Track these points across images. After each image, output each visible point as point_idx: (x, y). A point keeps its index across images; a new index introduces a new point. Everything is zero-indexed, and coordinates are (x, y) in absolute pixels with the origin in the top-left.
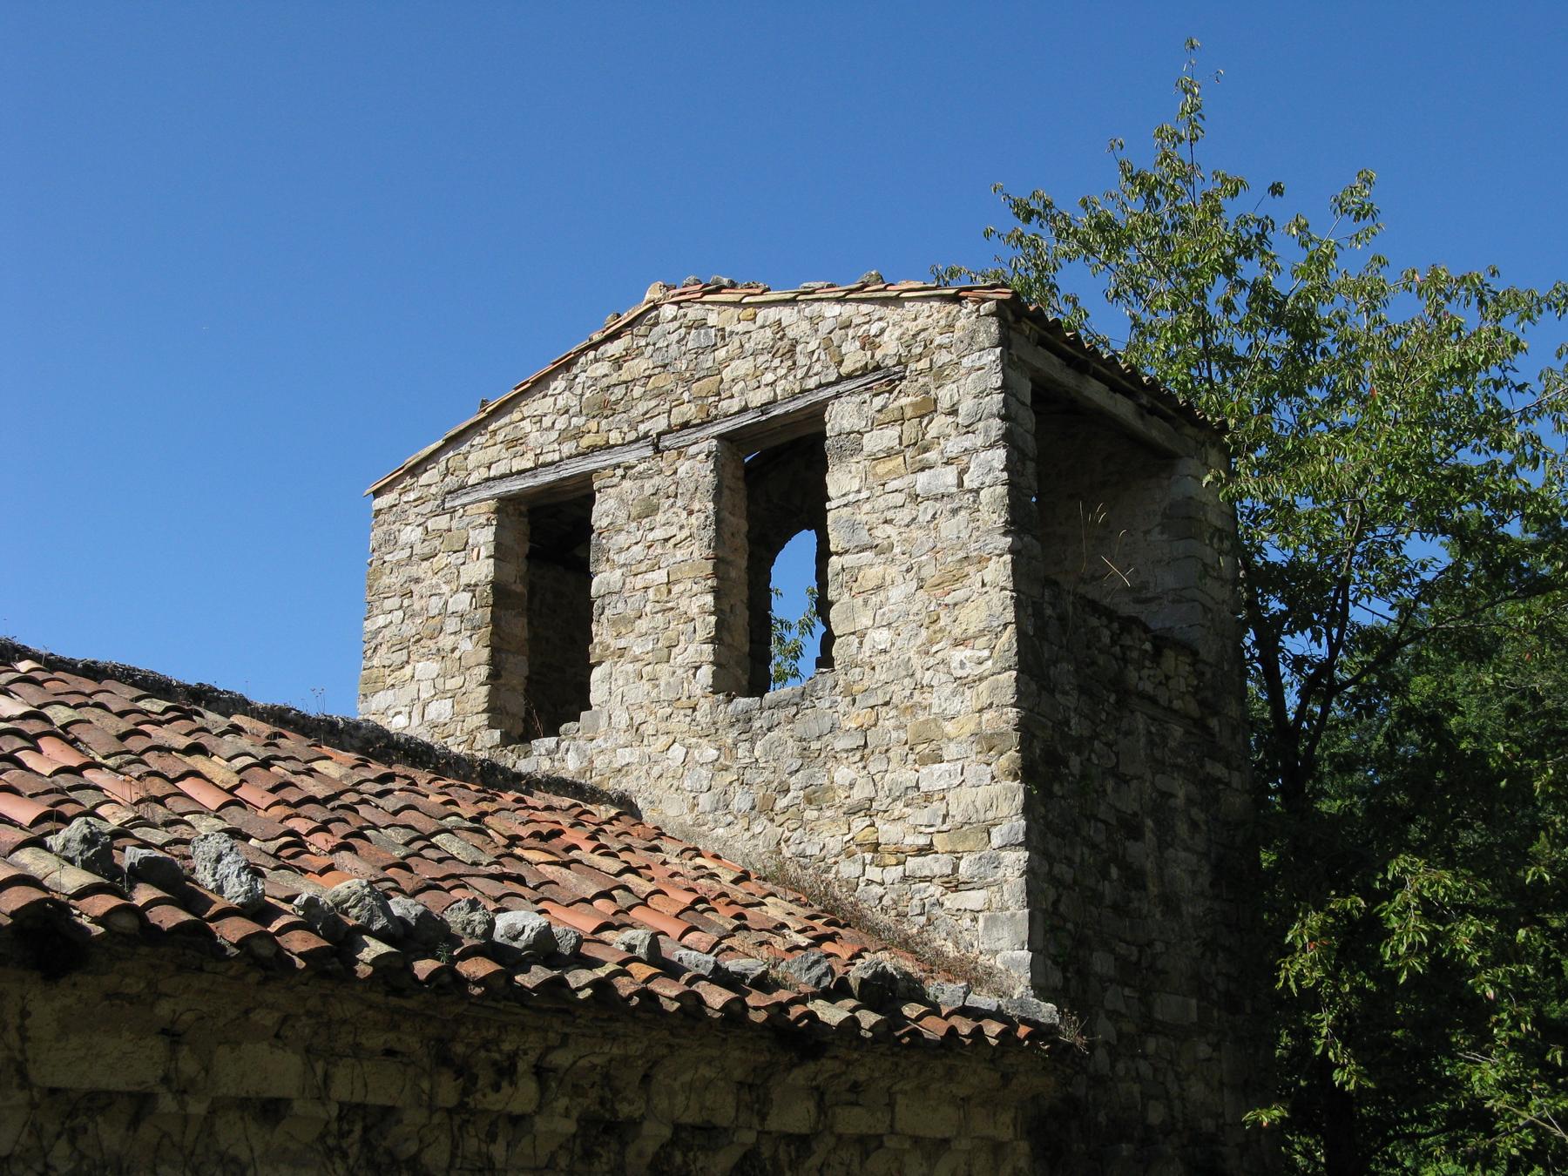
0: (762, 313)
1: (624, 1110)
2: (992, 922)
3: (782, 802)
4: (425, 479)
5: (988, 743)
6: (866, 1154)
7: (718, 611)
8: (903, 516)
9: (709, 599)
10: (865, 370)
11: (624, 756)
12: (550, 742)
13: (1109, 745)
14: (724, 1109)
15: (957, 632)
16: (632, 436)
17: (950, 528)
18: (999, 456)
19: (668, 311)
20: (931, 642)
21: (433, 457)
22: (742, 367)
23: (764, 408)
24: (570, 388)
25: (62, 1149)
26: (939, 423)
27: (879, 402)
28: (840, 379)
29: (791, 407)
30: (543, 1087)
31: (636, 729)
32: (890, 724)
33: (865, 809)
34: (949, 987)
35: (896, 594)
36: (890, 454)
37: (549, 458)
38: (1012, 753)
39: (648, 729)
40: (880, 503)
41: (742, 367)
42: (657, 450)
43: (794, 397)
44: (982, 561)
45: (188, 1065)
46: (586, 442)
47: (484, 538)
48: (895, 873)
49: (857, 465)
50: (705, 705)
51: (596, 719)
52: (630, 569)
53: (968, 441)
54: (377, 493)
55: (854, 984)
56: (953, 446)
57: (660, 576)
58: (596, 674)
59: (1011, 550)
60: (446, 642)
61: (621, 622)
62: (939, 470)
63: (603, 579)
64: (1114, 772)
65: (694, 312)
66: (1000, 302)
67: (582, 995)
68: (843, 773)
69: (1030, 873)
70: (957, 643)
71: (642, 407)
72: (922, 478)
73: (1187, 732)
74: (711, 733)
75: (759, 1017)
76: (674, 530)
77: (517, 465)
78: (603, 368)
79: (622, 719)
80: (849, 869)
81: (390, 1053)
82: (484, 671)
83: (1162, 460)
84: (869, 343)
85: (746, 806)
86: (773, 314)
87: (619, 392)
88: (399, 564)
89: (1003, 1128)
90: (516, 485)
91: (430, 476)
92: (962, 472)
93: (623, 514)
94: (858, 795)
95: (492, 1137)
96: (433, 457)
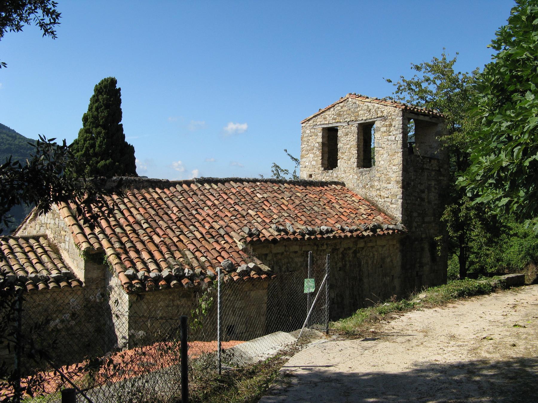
0: (365, 103)
1: (337, 247)
2: (396, 210)
3: (367, 187)
4: (310, 122)
5: (397, 182)
6: (372, 248)
7: (358, 154)
8: (386, 143)
9: (356, 152)
10: (381, 117)
11: (343, 175)
12: (331, 171)
13: (419, 179)
14: (351, 245)
15: (394, 164)
16: (344, 121)
17: (393, 146)
18: (401, 135)
19: (350, 99)
20: (390, 165)
21: (311, 118)
22: (362, 112)
23: (365, 120)
24: (334, 110)
25: (275, 258)
26: (392, 129)
27: (383, 123)
28: (377, 117)
29: (370, 121)
30: (327, 246)
31: (345, 171)
32: (383, 177)
33: (379, 190)
34: (385, 225)
35: (385, 156)
36: (385, 132)
37: (331, 122)
38: (401, 184)
39: (347, 172)
40: (383, 140)
41: (362, 112)
42: (348, 124)
43: (370, 119)
44: (398, 153)
45: (287, 249)
46: (336, 121)
47: (320, 134)
48: (383, 200)
49: (379, 133)
50: (355, 169)
51: (339, 168)
52: (344, 144)
53: (397, 132)
54: (302, 123)
55: (370, 228)
56: (394, 133)
57: (349, 146)
58: (339, 161)
59: (402, 152)
60: (314, 151)
61: (342, 153)
62: (392, 136)
63: (340, 145)
64: (420, 183)
65: (354, 101)
66: (402, 109)
67: (331, 238)
68: (376, 183)
69: (403, 203)
70: (393, 165)
71: (345, 117)
72: (389, 137)
73: (436, 173)
74: (356, 174)
75: (355, 236)
76: (351, 139)
77: (325, 123)
78: (339, 108)
79: (343, 169)
80: (376, 199)
81: (309, 244)
82: (320, 158)
83: (436, 124)
84: (382, 112)
85: (361, 186)
86: (367, 104)
87: (342, 113)
88: (306, 137)
89: (395, 242)
90: (325, 126)
91: (311, 122)
92: (395, 137)
93: (343, 134)
94: (378, 187)
95: (321, 252)
96: (311, 118)
